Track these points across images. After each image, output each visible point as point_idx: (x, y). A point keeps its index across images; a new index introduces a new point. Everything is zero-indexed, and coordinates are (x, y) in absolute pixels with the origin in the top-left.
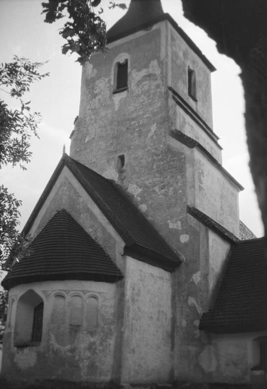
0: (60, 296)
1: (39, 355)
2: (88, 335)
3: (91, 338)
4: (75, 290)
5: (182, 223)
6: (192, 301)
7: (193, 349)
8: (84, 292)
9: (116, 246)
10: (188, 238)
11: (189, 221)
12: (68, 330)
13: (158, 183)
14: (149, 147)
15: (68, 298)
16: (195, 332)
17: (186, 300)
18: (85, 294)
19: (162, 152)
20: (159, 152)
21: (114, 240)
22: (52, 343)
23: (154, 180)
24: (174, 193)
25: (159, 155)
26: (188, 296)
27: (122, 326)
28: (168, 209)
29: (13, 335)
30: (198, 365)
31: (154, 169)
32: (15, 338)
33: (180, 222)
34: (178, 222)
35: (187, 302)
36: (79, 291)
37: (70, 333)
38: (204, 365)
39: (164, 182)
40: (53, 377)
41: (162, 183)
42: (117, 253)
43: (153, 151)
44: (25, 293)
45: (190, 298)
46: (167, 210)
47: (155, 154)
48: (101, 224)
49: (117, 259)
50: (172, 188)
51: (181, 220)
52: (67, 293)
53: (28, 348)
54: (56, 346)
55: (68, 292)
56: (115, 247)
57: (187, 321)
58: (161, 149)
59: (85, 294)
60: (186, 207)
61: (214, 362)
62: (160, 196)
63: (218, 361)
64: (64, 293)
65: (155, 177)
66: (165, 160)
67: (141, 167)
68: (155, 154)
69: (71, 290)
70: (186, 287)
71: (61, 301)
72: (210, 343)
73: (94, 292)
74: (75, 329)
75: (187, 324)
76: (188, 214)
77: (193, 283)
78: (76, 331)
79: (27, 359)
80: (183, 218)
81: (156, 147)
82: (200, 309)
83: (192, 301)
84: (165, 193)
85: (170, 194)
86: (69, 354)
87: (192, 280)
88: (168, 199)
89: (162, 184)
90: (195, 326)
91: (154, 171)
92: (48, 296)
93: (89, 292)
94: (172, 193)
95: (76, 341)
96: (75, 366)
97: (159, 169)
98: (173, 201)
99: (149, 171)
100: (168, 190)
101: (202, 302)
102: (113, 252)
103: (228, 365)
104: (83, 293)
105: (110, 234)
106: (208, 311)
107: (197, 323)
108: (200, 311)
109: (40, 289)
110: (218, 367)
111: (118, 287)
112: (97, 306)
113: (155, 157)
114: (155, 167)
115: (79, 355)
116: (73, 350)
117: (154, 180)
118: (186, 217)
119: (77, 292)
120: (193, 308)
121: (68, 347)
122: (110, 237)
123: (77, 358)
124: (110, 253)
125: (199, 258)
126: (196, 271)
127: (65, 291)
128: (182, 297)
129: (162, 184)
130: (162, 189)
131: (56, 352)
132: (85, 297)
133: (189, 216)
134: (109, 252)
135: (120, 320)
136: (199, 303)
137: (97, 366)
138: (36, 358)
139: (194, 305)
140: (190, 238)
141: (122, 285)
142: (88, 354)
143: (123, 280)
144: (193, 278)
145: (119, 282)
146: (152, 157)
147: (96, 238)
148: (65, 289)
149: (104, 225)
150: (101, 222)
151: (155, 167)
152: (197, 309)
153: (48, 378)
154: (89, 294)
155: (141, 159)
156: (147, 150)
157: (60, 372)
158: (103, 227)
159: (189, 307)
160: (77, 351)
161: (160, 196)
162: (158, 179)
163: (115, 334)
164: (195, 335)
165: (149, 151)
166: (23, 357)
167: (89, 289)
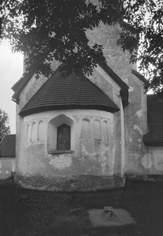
0: (86, 120)
1: (74, 159)
2: (105, 146)
3: (106, 148)
4: (96, 117)
5: (129, 79)
6: (136, 127)
7: (137, 155)
8: (101, 118)
9: (113, 89)
10: (133, 89)
11: (133, 79)
12: (94, 143)
13: (111, 52)
14: (103, 28)
15: (92, 121)
16: (138, 146)
17: (133, 126)
18: (102, 119)
19: (113, 32)
20: (110, 33)
21: (111, 85)
22: (83, 152)
23: (108, 50)
24: (123, 60)
25: (110, 34)
26: (133, 124)
27: (121, 141)
28: (118, 69)
29: (46, 146)
30: (140, 165)
31: (108, 43)
32: (48, 148)
33: (128, 79)
34: (126, 78)
35: (133, 128)
36: (98, 117)
37: (96, 144)
38: (144, 164)
39: (115, 52)
40: (86, 174)
41: (113, 52)
42: (113, 94)
43: (106, 31)
44: (56, 117)
45: (135, 125)
46: (118, 70)
47: (108, 33)
48: (100, 75)
49: (114, 98)
50: (121, 57)
51: (128, 77)
52: (91, 118)
53: (63, 155)
54: (87, 153)
55: (92, 117)
56: (112, 90)
57: (133, 139)
58: (112, 31)
59: (102, 119)
60: (131, 69)
61: (151, 163)
62: (113, 61)
63: (153, 162)
64: (89, 118)
65: (108, 48)
66: (115, 38)
67: (97, 40)
68: (108, 33)
69: (94, 116)
70: (132, 118)
71: (86, 123)
72: (148, 152)
73: (106, 118)
74: (98, 142)
75: (133, 141)
76: (132, 74)
77: (137, 116)
78: (99, 144)
79: (62, 162)
80: (129, 77)
81: (108, 29)
82: (142, 132)
83: (136, 127)
84: (116, 59)
85: (120, 60)
86: (95, 158)
87: (136, 115)
88: (118, 63)
89: (114, 53)
90: (138, 142)
91: (107, 44)
92: (78, 120)
93: (104, 118)
94: (121, 60)
95: (99, 149)
96: (98, 165)
97: (111, 43)
98: (122, 65)
99: (103, 43)
100: (118, 58)
101: (143, 128)
102: (110, 93)
103: (159, 164)
104: (101, 118)
105: (107, 82)
106: (146, 134)
107: (140, 140)
108: (142, 133)
109: (70, 114)
110: (153, 165)
111: (116, 116)
112: (107, 127)
113: (108, 35)
114: (108, 41)
115: (101, 159)
116: (97, 156)
117: (108, 50)
118: (132, 76)
119: (97, 118)
120: (137, 132)
121: (95, 154)
122: (107, 83)
123: (100, 161)
124: (108, 94)
125: (141, 101)
126: (139, 109)
127: (90, 116)
128: (129, 125)
129: (114, 53)
130: (114, 56)
131: (86, 157)
132: (102, 121)
133: (133, 75)
134: (107, 93)
135: (118, 137)
136: (141, 129)
137: (109, 166)
138: (71, 161)
139: (138, 129)
140: (134, 89)
141: (119, 115)
142: (105, 158)
143: (119, 111)
144: (137, 113)
145: (116, 113)
146: (106, 35)
147: (96, 83)
148: (90, 115)
149: (102, 75)
150: (100, 73)
151: (108, 41)
152: (140, 132)
153: (82, 174)
154: (94, 118)
155: (97, 35)
156: (101, 29)
157: (90, 170)
158: (102, 76)
159: (135, 131)
160: (100, 156)
161: (113, 61)
162: (110, 50)
163: (115, 146)
164: (139, 147)
165: (102, 30)
166: (60, 161)
167: (104, 117)
